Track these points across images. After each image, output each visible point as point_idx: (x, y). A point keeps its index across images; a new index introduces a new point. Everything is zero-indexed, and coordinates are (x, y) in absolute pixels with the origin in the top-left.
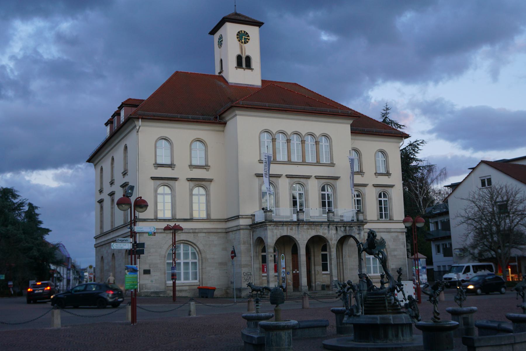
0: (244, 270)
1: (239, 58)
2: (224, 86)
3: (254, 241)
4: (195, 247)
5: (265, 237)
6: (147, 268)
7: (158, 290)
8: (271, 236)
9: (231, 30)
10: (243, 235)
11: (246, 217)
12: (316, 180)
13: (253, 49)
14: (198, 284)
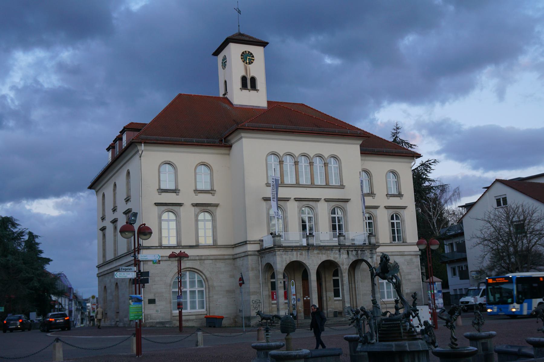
0: (253, 298)
1: (244, 79)
2: (229, 108)
4: (201, 274)
5: (274, 263)
6: (151, 297)
7: (163, 321)
8: (281, 262)
9: (235, 51)
10: (251, 261)
11: (254, 242)
12: (326, 203)
13: (258, 70)
14: (205, 313)
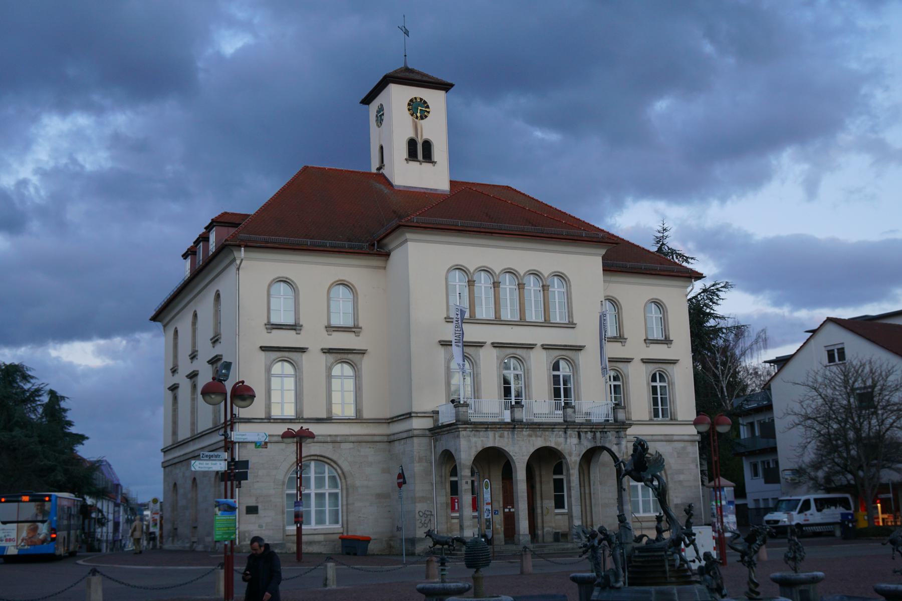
0: (420, 507)
1: (412, 143)
3: (438, 456)
4: (335, 466)
5: (456, 450)
6: (252, 502)
8: (467, 448)
9: (398, 97)
10: (419, 446)
11: (424, 415)
12: (544, 352)
13: (435, 129)
14: (341, 531)
